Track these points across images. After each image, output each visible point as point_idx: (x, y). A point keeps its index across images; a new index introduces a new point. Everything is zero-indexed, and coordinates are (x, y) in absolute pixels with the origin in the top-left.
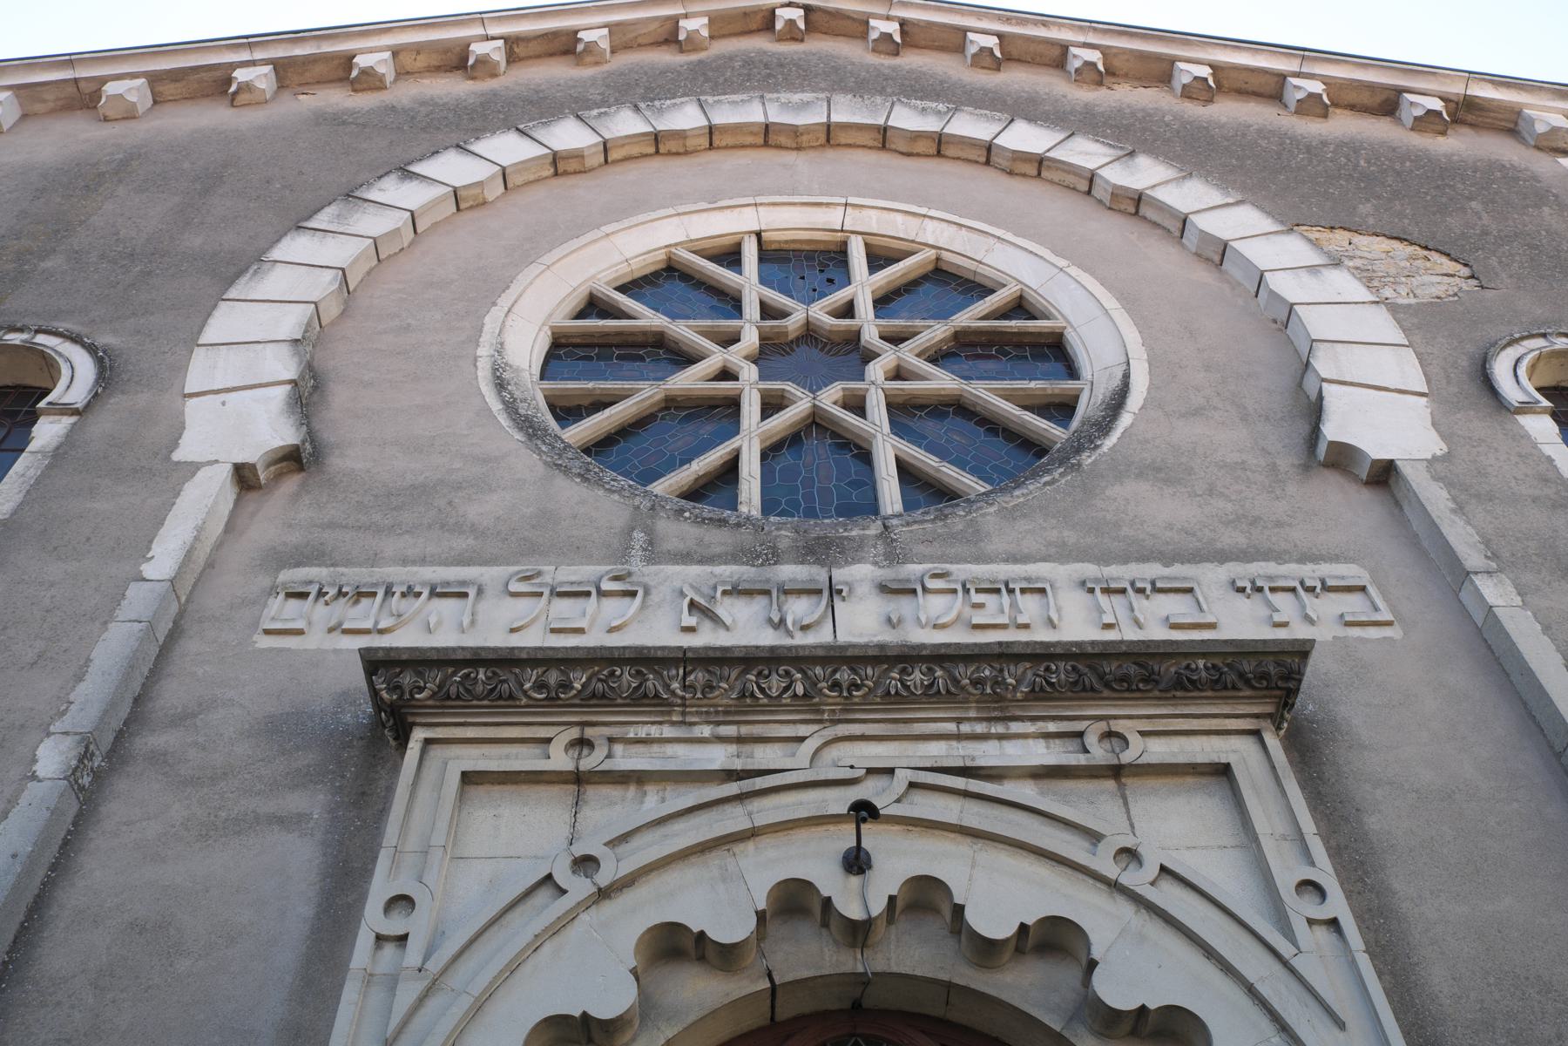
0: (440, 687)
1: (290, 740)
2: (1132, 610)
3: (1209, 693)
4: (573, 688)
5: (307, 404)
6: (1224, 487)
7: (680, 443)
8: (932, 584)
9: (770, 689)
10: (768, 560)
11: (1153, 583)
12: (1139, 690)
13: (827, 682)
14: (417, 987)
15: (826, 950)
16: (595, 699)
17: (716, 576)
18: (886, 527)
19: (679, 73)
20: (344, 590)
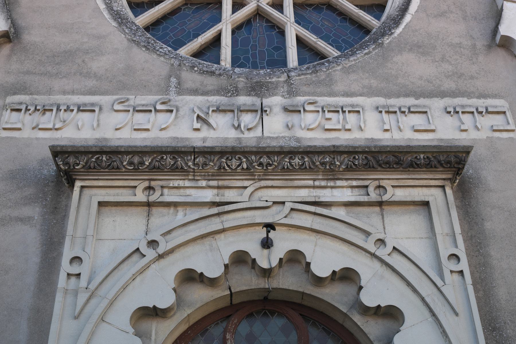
0: (86, 163)
1: (21, 182)
2: (398, 122)
3: (424, 169)
4: (145, 164)
5: (9, 4)
6: (450, 57)
7: (193, 24)
8: (308, 108)
9: (232, 165)
10: (233, 93)
12: (393, 168)
13: (257, 163)
14: (86, 296)
15: (253, 278)
16: (154, 169)
17: (209, 102)
18: (289, 77)
20: (38, 108)
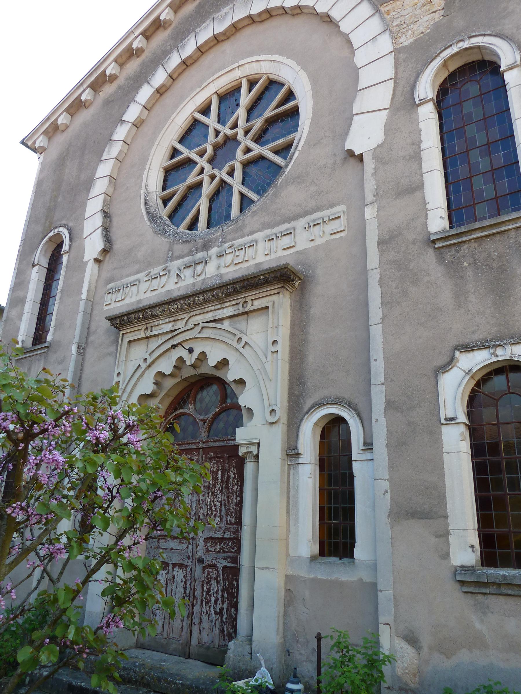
12: (248, 289)
16: (145, 318)
19: (192, 15)
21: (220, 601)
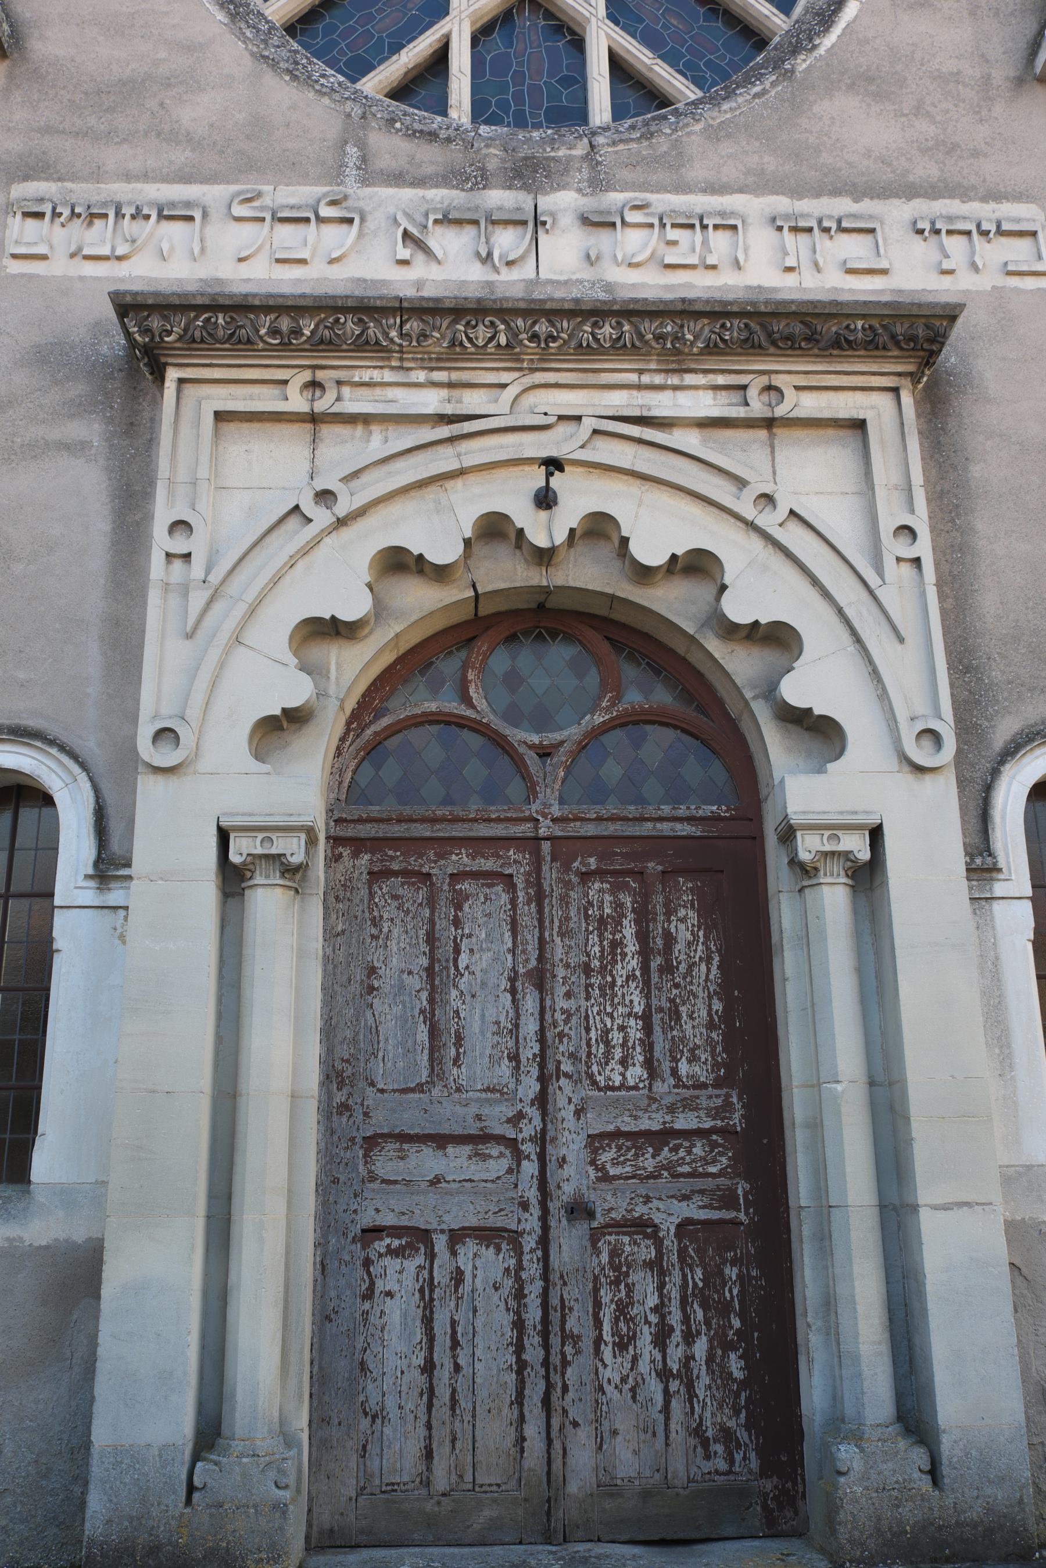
0: (185, 330)
1: (59, 371)
2: (815, 252)
3: (862, 353)
4: (303, 334)
9: (477, 338)
11: (839, 222)
12: (800, 348)
14: (205, 595)
15: (518, 567)
16: (322, 344)
17: (427, 201)
21: (677, 1337)
